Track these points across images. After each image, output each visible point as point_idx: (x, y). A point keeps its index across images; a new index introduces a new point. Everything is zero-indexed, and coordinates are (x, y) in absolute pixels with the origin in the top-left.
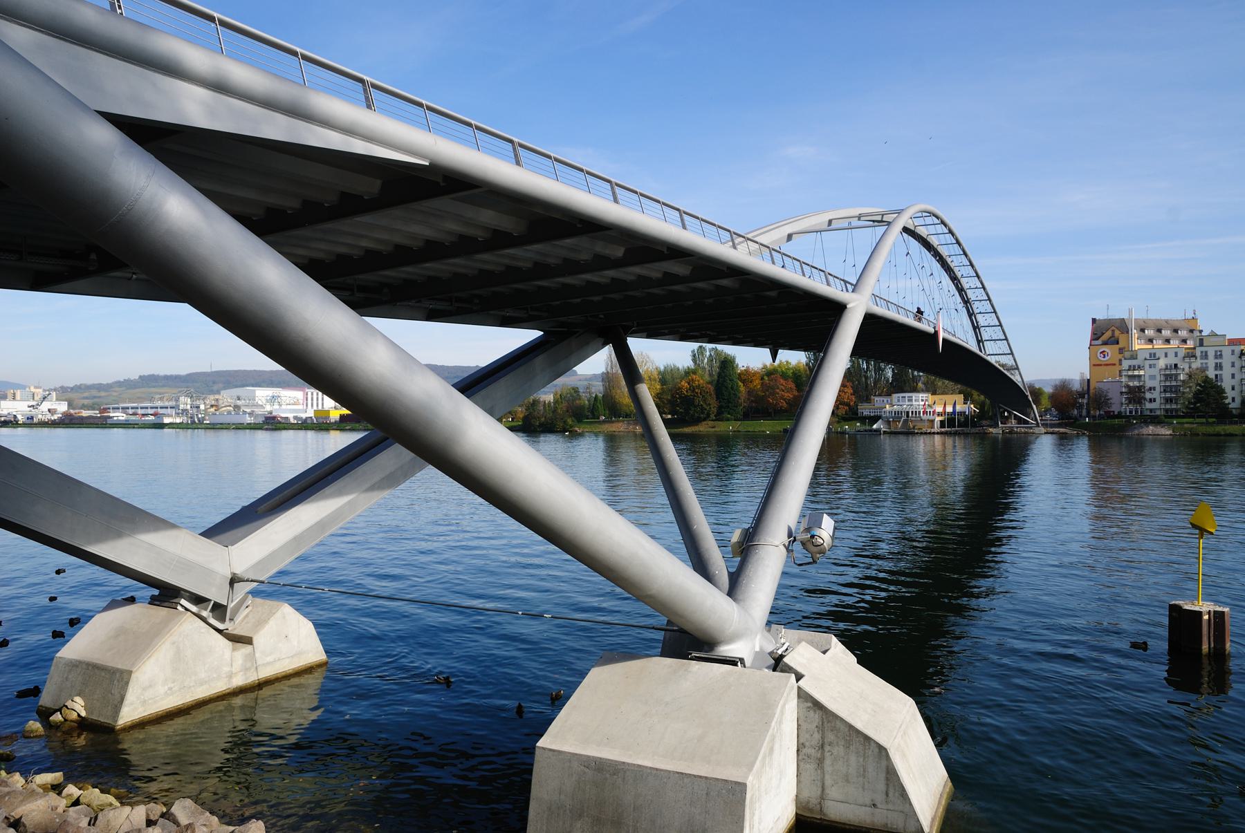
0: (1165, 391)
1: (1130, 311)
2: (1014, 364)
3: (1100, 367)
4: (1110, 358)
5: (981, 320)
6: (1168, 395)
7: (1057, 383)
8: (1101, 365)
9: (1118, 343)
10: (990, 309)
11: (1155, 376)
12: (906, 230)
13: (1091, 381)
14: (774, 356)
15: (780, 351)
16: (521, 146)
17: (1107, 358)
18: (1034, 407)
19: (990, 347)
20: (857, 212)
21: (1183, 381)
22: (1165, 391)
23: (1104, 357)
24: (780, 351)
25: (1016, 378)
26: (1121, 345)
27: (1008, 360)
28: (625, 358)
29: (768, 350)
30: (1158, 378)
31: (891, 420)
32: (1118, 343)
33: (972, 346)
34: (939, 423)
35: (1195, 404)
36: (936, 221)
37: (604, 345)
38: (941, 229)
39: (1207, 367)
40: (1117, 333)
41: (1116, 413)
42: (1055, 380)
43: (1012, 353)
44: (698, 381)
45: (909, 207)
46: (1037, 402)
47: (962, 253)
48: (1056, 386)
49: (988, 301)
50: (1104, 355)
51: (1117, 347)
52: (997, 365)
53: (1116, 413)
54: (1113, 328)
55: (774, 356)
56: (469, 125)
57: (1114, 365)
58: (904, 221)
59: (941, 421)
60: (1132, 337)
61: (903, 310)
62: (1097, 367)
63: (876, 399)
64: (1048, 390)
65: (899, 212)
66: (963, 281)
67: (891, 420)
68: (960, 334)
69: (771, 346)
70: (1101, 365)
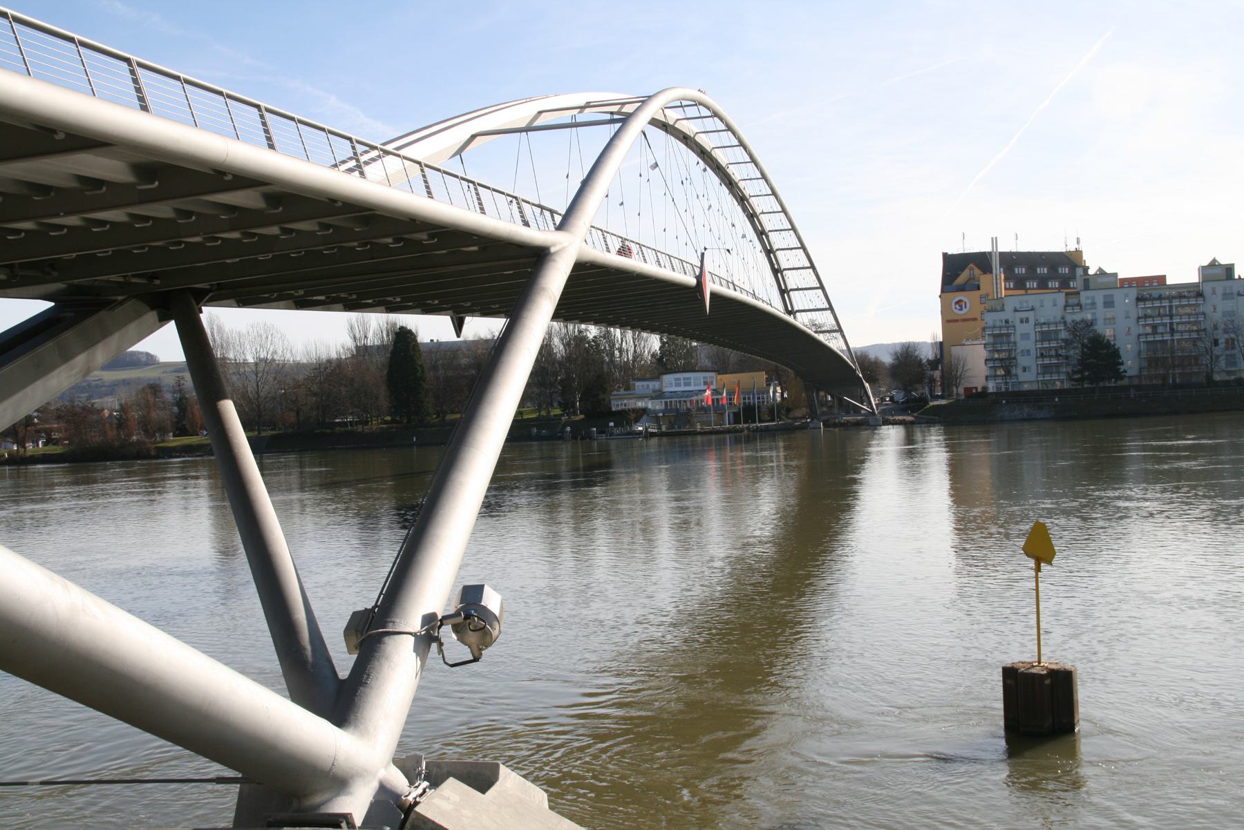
0: (1042, 356)
1: (994, 241)
2: (834, 322)
3: (956, 324)
4: (969, 311)
5: (784, 259)
6: (1047, 361)
7: (898, 349)
8: (957, 321)
9: (978, 288)
10: (722, 127)
11: (1028, 334)
12: (654, 122)
13: (945, 346)
14: (459, 326)
15: (468, 319)
16: (141, 65)
17: (965, 311)
18: (867, 385)
19: (798, 300)
20: (580, 99)
21: (1065, 341)
22: (1042, 356)
23: (961, 309)
24: (468, 319)
25: (835, 344)
26: (983, 291)
27: (825, 319)
28: (194, 338)
29: (449, 317)
30: (1032, 336)
31: (661, 414)
32: (978, 288)
33: (777, 308)
34: (731, 415)
35: (1080, 372)
36: (705, 112)
37: (163, 320)
38: (728, 138)
39: (1096, 320)
40: (977, 271)
41: (979, 390)
42: (895, 344)
43: (831, 308)
44: (533, 392)
45: (664, 90)
46: (871, 380)
47: (760, 176)
48: (896, 354)
49: (811, 270)
50: (961, 306)
51: (976, 294)
52: (839, 352)
53: (979, 390)
54: (971, 265)
55: (459, 326)
56: (71, 40)
57: (975, 319)
58: (652, 110)
59: (734, 413)
60: (996, 279)
61: (663, 255)
62: (951, 324)
63: (637, 384)
64: (887, 359)
65: (644, 101)
66: (732, 170)
67: (661, 414)
68: (761, 293)
69: (451, 312)
70: (957, 321)
